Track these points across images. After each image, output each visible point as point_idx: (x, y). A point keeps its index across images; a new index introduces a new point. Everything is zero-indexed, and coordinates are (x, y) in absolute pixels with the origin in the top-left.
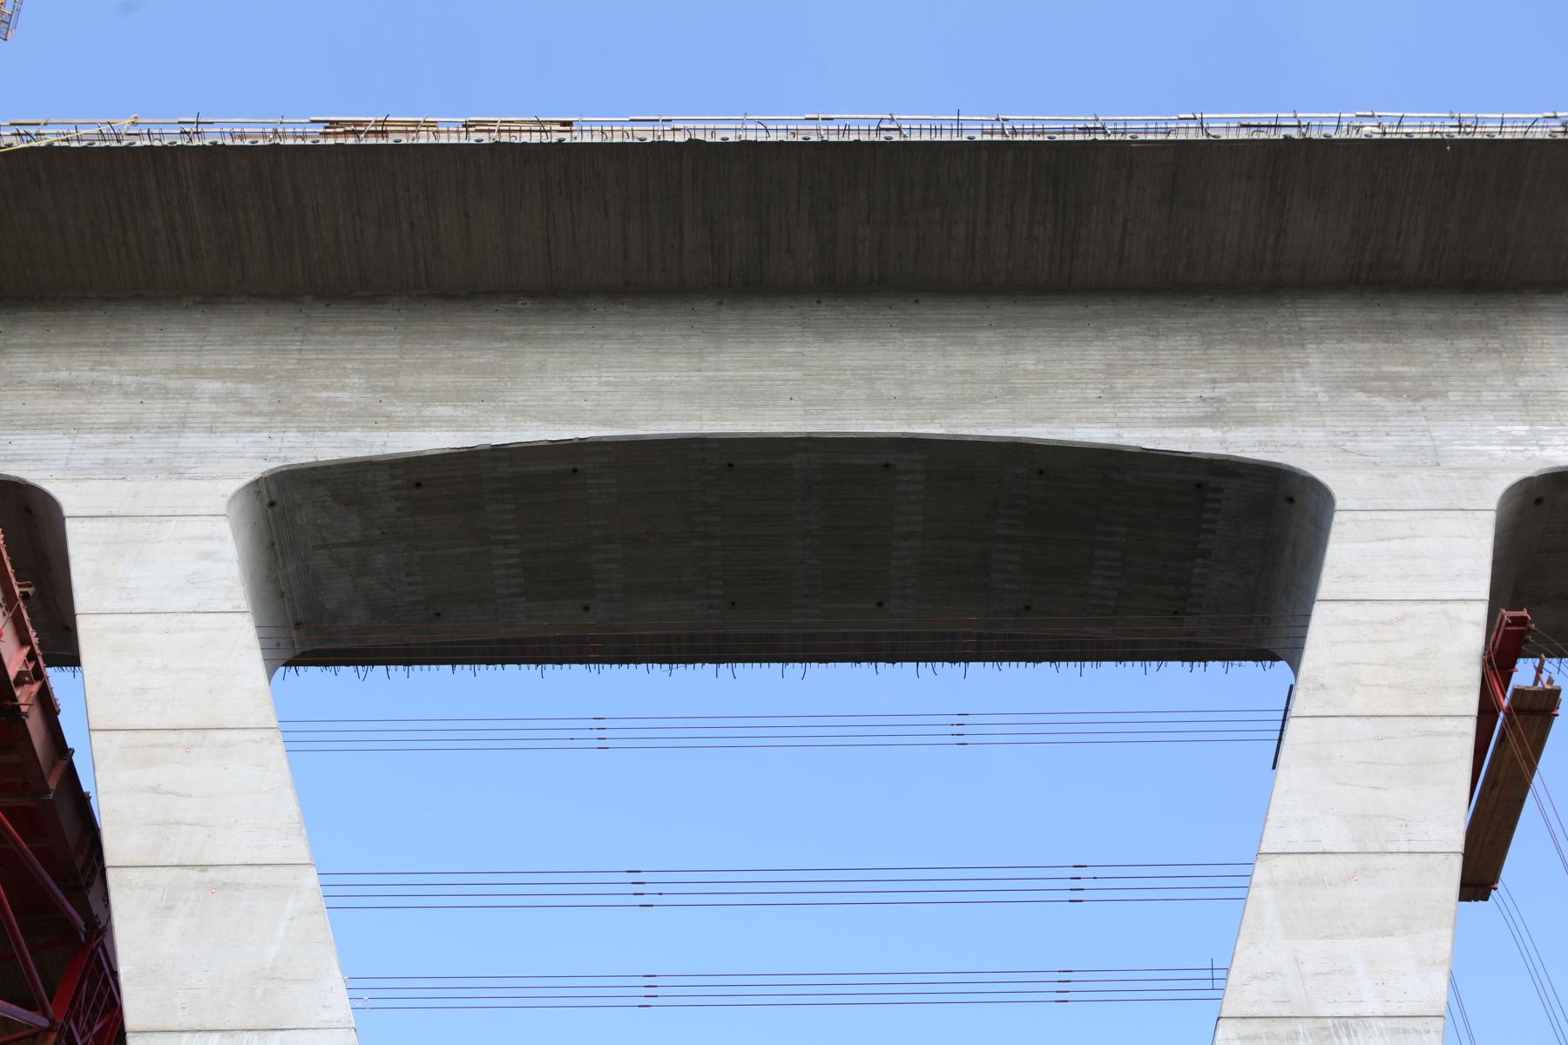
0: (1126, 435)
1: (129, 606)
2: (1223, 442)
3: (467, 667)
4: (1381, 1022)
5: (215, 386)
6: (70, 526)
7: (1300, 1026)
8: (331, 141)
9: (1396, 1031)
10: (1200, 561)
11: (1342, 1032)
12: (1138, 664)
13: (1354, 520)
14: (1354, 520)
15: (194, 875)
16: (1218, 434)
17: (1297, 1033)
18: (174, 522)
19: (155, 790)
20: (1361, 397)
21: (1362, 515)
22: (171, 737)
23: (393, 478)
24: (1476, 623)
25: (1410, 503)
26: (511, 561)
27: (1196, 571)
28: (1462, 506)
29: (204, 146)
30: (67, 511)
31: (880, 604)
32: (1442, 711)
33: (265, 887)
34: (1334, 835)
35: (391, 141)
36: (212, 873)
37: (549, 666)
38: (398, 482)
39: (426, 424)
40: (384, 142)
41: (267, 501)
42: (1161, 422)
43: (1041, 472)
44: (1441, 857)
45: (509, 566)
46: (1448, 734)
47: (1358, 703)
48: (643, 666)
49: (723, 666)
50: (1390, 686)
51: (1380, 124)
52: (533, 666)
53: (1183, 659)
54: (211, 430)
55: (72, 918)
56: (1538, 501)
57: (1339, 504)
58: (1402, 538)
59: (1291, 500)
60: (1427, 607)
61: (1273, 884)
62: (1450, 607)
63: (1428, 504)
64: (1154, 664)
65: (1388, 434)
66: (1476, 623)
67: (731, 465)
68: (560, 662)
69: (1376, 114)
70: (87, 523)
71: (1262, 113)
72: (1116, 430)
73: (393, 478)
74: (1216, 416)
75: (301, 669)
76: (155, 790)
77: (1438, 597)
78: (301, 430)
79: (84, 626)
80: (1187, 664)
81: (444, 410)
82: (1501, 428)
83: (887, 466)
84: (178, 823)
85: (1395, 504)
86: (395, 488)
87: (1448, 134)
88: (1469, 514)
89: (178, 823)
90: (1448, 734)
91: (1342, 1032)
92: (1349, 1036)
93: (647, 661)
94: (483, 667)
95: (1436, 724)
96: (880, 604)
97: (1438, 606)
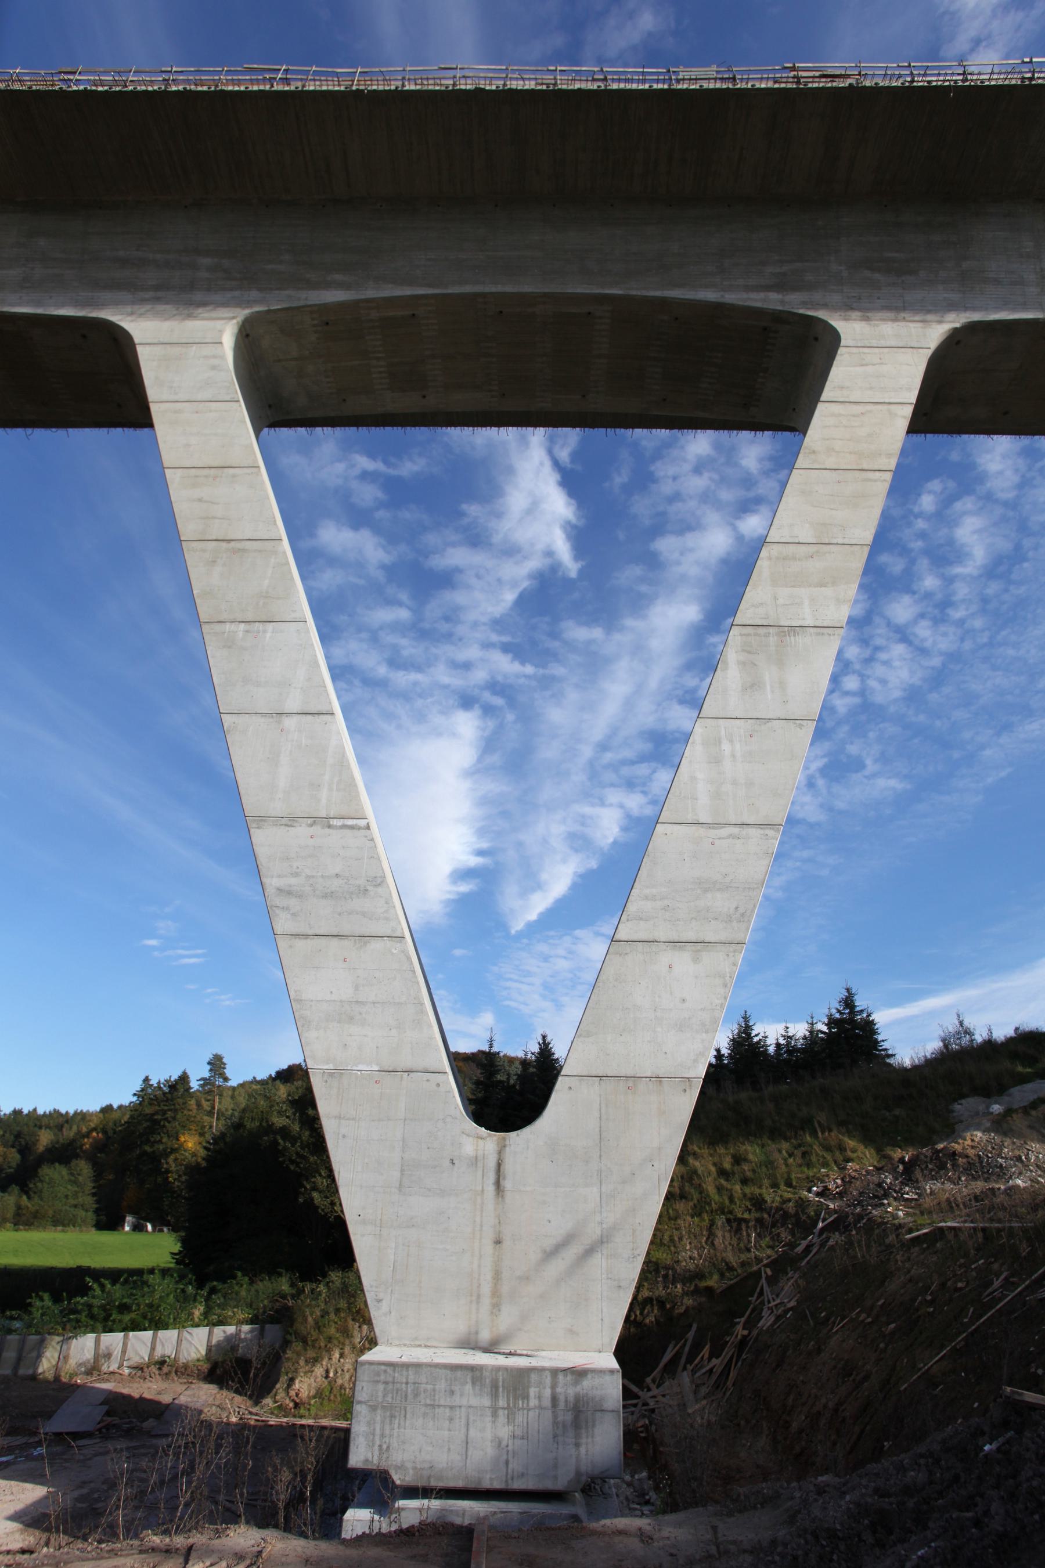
0: (727, 296)
1: (176, 398)
2: (782, 302)
3: (365, 428)
4: (812, 630)
5: (207, 261)
6: (140, 349)
7: (771, 630)
8: (255, 88)
9: (818, 634)
10: (761, 374)
11: (792, 634)
12: (726, 431)
13: (849, 353)
14: (849, 353)
15: (224, 545)
16: (780, 296)
17: (769, 633)
18: (195, 347)
19: (200, 500)
20: (867, 273)
21: (854, 350)
22: (206, 472)
23: (313, 319)
24: (905, 417)
25: (883, 343)
26: (382, 369)
27: (760, 380)
28: (912, 346)
29: (179, 91)
30: (136, 341)
31: (584, 396)
32: (876, 468)
33: (260, 551)
34: (805, 534)
35: (293, 88)
36: (233, 544)
37: (408, 428)
38: (315, 322)
39: (328, 285)
40: (287, 88)
41: (244, 334)
42: (748, 289)
43: (677, 319)
44: (859, 547)
45: (380, 372)
46: (875, 481)
47: (830, 462)
48: (459, 428)
49: (502, 429)
50: (851, 453)
51: (860, 72)
52: (400, 428)
53: (751, 430)
54: (209, 290)
55: (719, 307)
56: (958, 343)
57: (843, 343)
58: (874, 365)
59: (816, 339)
60: (880, 407)
61: (770, 559)
62: (892, 407)
63: (893, 344)
64: (735, 432)
65: (879, 298)
66: (905, 417)
67: (501, 312)
68: (414, 426)
69: (912, 64)
70: (148, 348)
71: (760, 66)
72: (722, 293)
73: (313, 319)
74: (781, 285)
75: (277, 429)
76: (200, 500)
77: (887, 401)
78: (260, 290)
79: (154, 408)
80: (753, 432)
81: (338, 277)
82: (945, 295)
83: (589, 313)
84: (214, 518)
85: (874, 343)
86: (314, 326)
87: (956, 81)
88: (915, 351)
89: (214, 518)
90: (875, 481)
91: (792, 634)
92: (794, 636)
93: (461, 426)
94: (373, 428)
95: (871, 475)
96: (584, 396)
97: (886, 407)
